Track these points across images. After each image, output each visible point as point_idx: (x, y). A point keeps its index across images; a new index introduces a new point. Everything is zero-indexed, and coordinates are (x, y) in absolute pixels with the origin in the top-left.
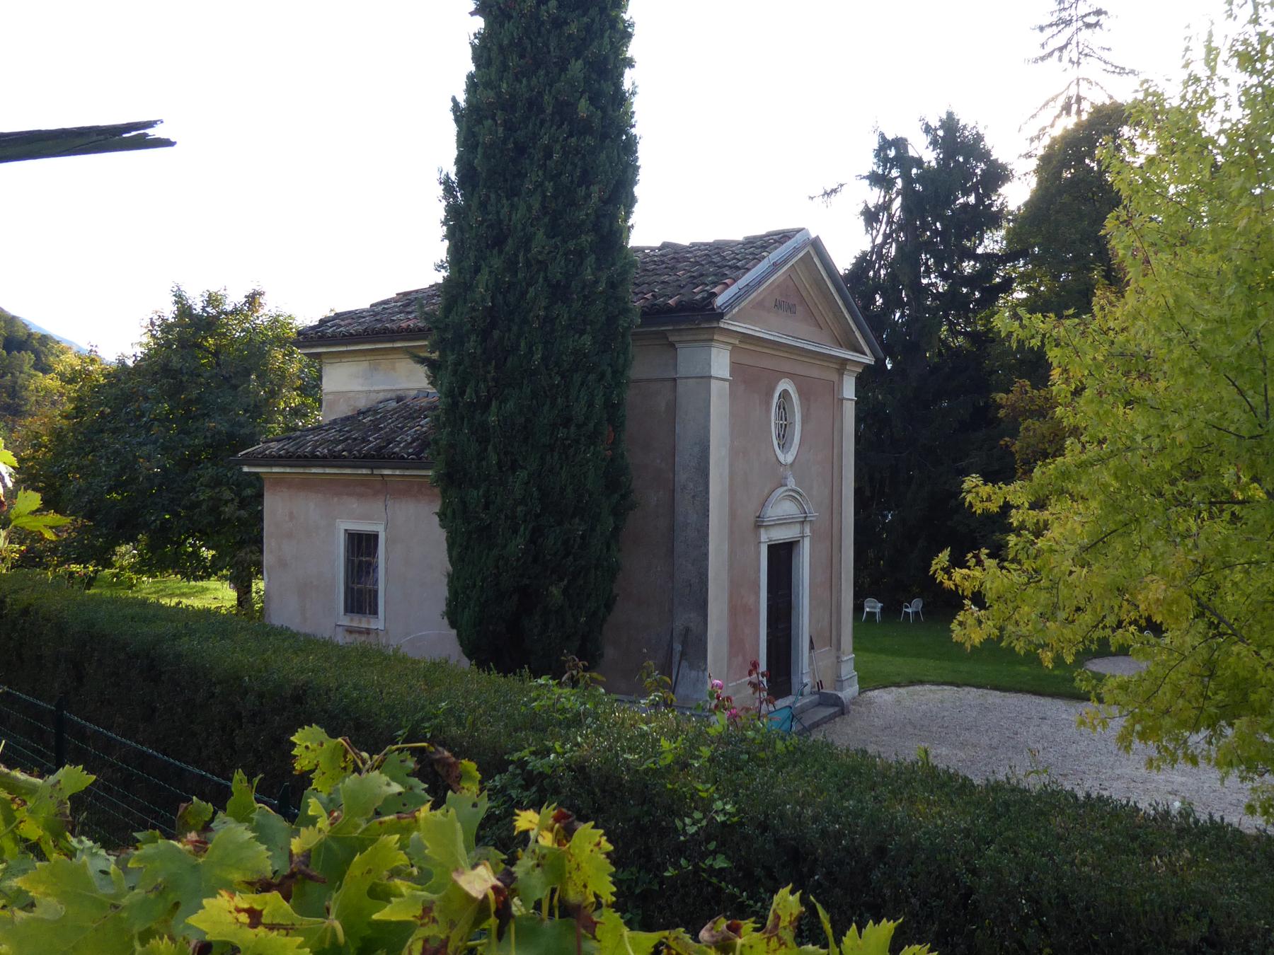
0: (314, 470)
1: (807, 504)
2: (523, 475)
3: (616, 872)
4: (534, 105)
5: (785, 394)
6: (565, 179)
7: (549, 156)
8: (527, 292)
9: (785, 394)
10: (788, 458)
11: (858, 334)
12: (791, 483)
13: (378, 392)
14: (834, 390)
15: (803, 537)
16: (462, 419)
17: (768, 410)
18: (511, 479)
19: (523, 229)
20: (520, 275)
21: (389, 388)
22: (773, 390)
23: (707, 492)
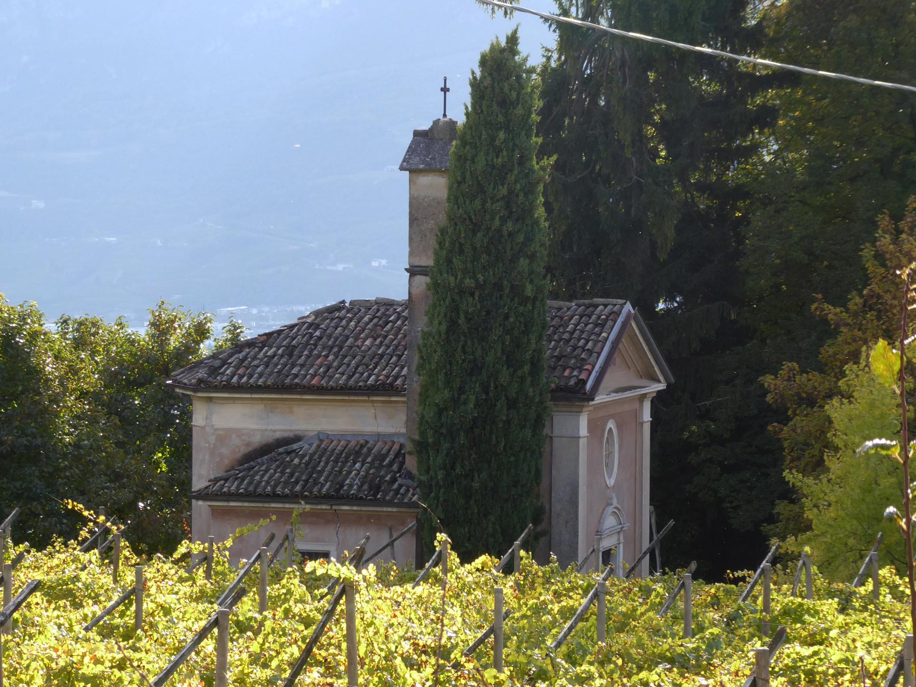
0: (273, 505)
1: (623, 517)
2: (492, 518)
3: (775, 535)
4: (498, 287)
5: (610, 429)
6: (516, 333)
7: (507, 317)
8: (495, 405)
9: (610, 429)
10: (611, 482)
11: (656, 368)
12: (615, 502)
13: (274, 431)
14: (637, 414)
15: (619, 544)
16: (453, 483)
17: (602, 448)
18: (484, 521)
19: (493, 367)
20: (491, 395)
21: (289, 428)
22: (604, 430)
23: (577, 519)
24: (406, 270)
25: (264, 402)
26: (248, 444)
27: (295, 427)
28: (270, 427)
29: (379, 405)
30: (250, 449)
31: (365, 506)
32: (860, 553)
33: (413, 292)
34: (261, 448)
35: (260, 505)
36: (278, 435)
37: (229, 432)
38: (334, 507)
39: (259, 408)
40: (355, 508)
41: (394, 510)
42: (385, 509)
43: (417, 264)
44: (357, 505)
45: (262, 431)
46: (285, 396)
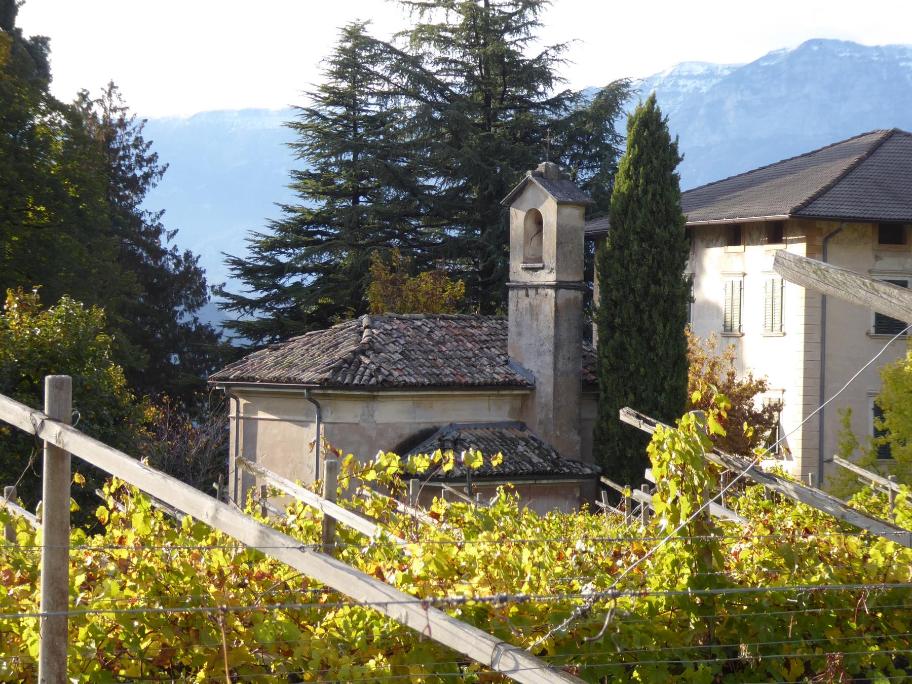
13: (419, 424)
24: (204, 272)
25: (414, 399)
26: (400, 436)
27: (433, 420)
28: (417, 420)
29: (493, 398)
30: (402, 440)
31: (558, 479)
32: (405, 488)
33: (559, 303)
34: (410, 439)
35: (487, 483)
36: (422, 427)
37: (388, 425)
38: (538, 482)
39: (408, 405)
40: (550, 481)
41: (575, 481)
42: (569, 481)
43: (561, 279)
44: (546, 479)
45: (411, 424)
46: (419, 393)
